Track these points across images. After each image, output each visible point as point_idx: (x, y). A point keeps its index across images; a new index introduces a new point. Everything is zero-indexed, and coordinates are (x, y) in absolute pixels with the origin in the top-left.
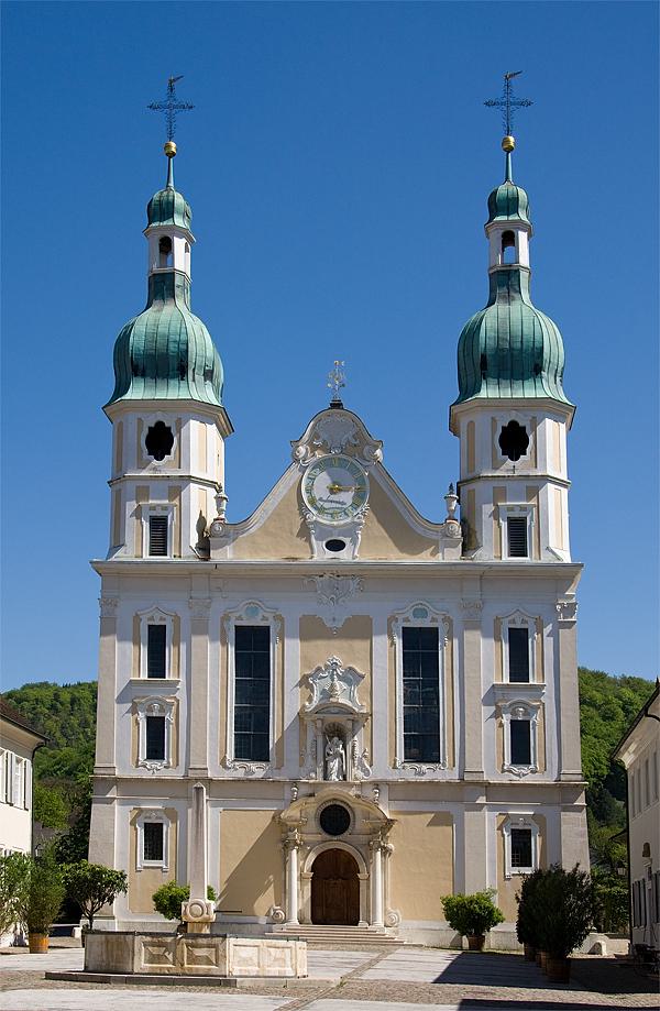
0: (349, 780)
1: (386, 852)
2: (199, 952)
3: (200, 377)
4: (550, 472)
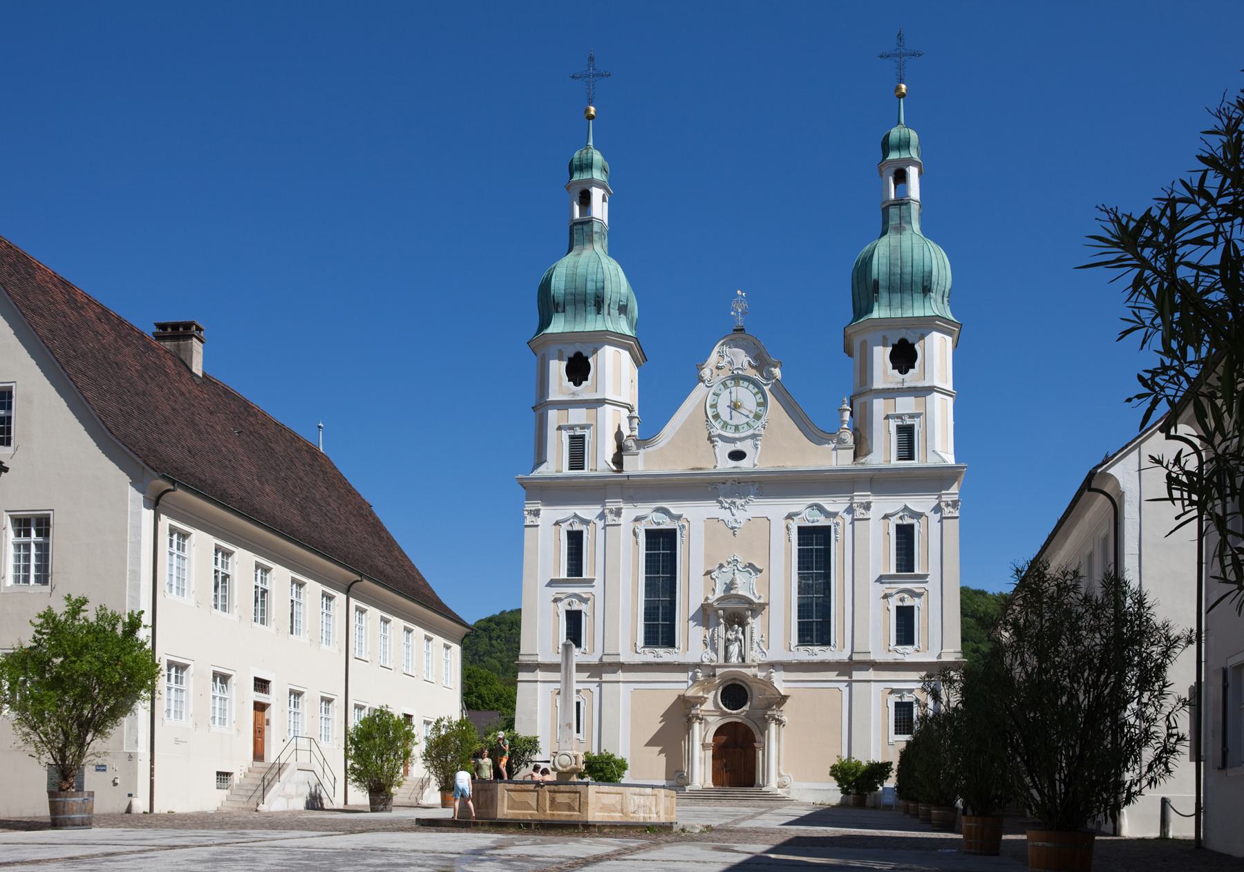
0: (748, 661)
1: (779, 722)
3: (614, 312)
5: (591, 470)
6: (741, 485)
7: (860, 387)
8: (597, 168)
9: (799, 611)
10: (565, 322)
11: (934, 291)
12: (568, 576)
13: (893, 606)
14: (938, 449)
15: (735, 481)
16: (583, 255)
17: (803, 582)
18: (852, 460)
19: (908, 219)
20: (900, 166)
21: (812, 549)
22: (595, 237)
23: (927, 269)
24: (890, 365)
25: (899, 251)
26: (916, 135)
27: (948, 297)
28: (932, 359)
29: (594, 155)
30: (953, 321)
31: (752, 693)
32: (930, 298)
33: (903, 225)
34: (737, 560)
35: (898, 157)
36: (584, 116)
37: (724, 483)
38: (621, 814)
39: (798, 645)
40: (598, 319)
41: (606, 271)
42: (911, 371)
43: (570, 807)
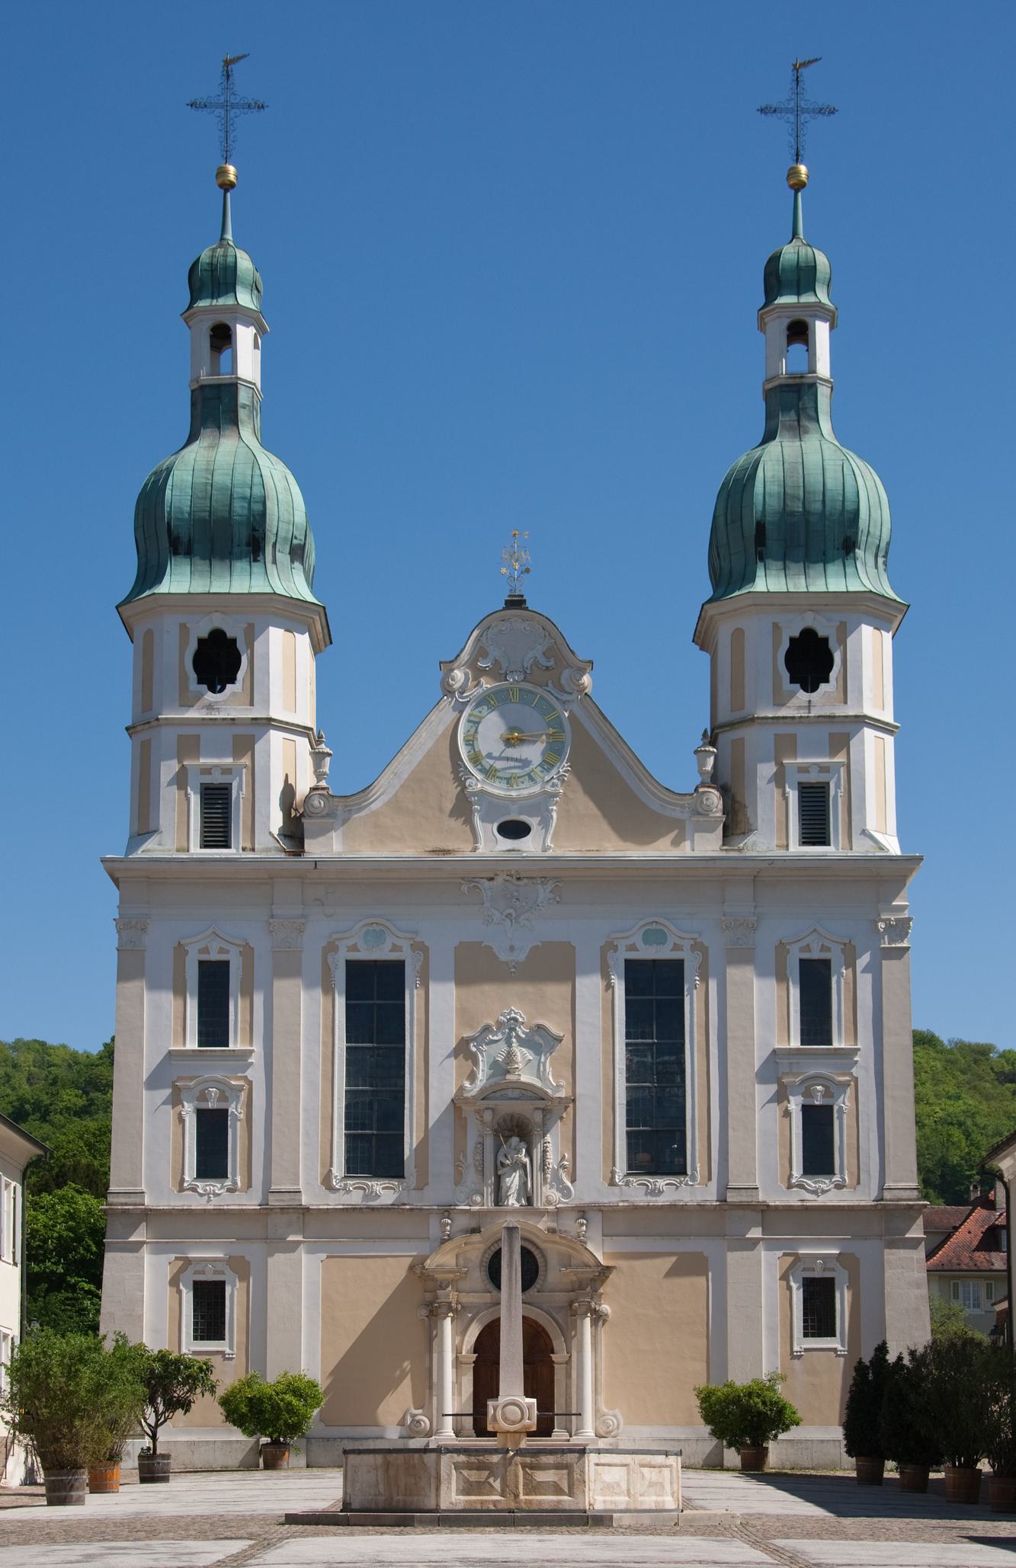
0: (538, 1204)
1: (598, 1318)
2: (541, 1476)
3: (283, 557)
5: (244, 849)
6: (521, 883)
7: (732, 711)
8: (244, 285)
9: (629, 1112)
11: (862, 547)
12: (199, 1046)
13: (796, 1105)
14: (871, 826)
15: (511, 876)
16: (221, 449)
17: (636, 1059)
18: (721, 842)
19: (812, 414)
20: (799, 315)
21: (652, 1000)
22: (242, 414)
23: (849, 506)
25: (802, 474)
26: (825, 260)
27: (884, 557)
28: (860, 667)
29: (239, 260)
30: (895, 600)
31: (545, 1261)
34: (515, 1020)
35: (796, 301)
36: (214, 184)
37: (491, 879)
38: (627, 1498)
39: (629, 1175)
40: (255, 569)
41: (268, 481)
42: (823, 687)
43: (558, 1490)
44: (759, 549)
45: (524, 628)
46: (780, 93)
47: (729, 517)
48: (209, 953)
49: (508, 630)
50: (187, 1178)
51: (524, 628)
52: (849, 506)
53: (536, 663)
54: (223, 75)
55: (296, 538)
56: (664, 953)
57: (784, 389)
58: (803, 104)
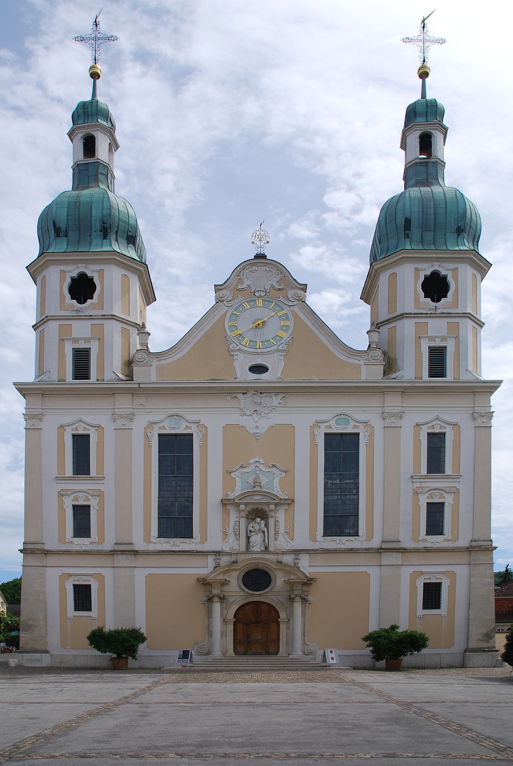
4: (117, 312)
6: (263, 395)
10: (67, 245)
11: (467, 233)
17: (329, 482)
23: (461, 211)
24: (422, 294)
32: (464, 238)
33: (429, 180)
42: (443, 300)
44: (406, 232)
45: (266, 269)
46: (415, 31)
47: (387, 220)
48: (78, 431)
49: (256, 270)
50: (67, 537)
51: (266, 269)
52: (461, 211)
53: (272, 286)
54: (94, 25)
55: (130, 232)
56: (349, 430)
57: (418, 164)
58: (427, 38)
